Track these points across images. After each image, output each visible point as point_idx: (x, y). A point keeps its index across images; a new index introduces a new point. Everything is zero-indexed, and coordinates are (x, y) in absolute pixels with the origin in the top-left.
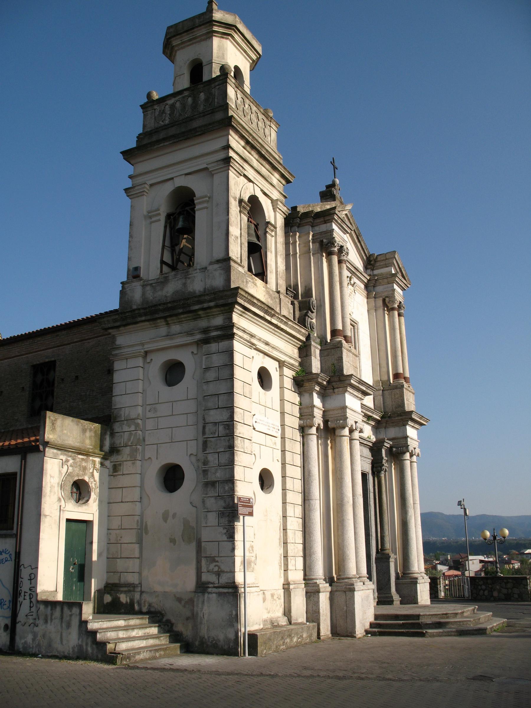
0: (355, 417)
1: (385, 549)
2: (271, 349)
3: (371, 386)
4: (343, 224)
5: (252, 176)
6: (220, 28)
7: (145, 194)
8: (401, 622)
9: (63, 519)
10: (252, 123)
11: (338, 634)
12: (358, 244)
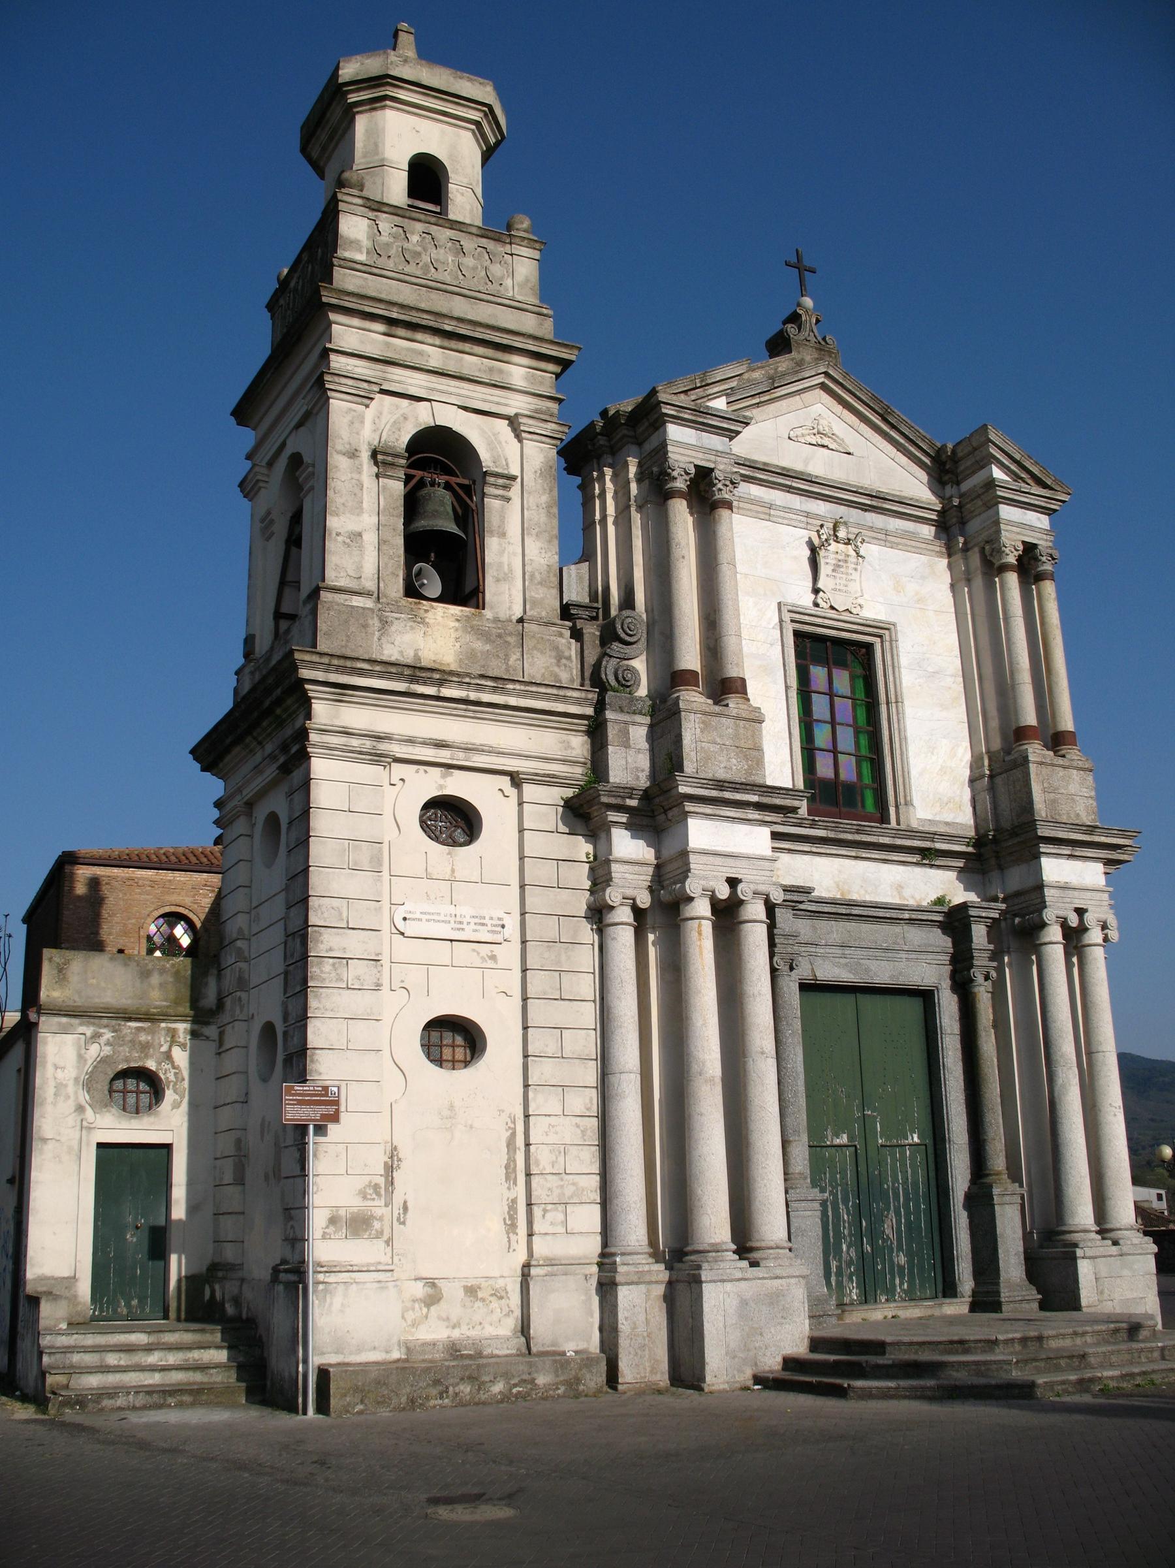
0: (724, 869)
1: (988, 1172)
2: (461, 755)
3: (791, 790)
4: (705, 418)
5: (421, 387)
6: (361, 93)
7: (261, 484)
8: (832, 1358)
9: (88, 1144)
10: (436, 269)
11: (682, 1381)
12: (893, 433)
